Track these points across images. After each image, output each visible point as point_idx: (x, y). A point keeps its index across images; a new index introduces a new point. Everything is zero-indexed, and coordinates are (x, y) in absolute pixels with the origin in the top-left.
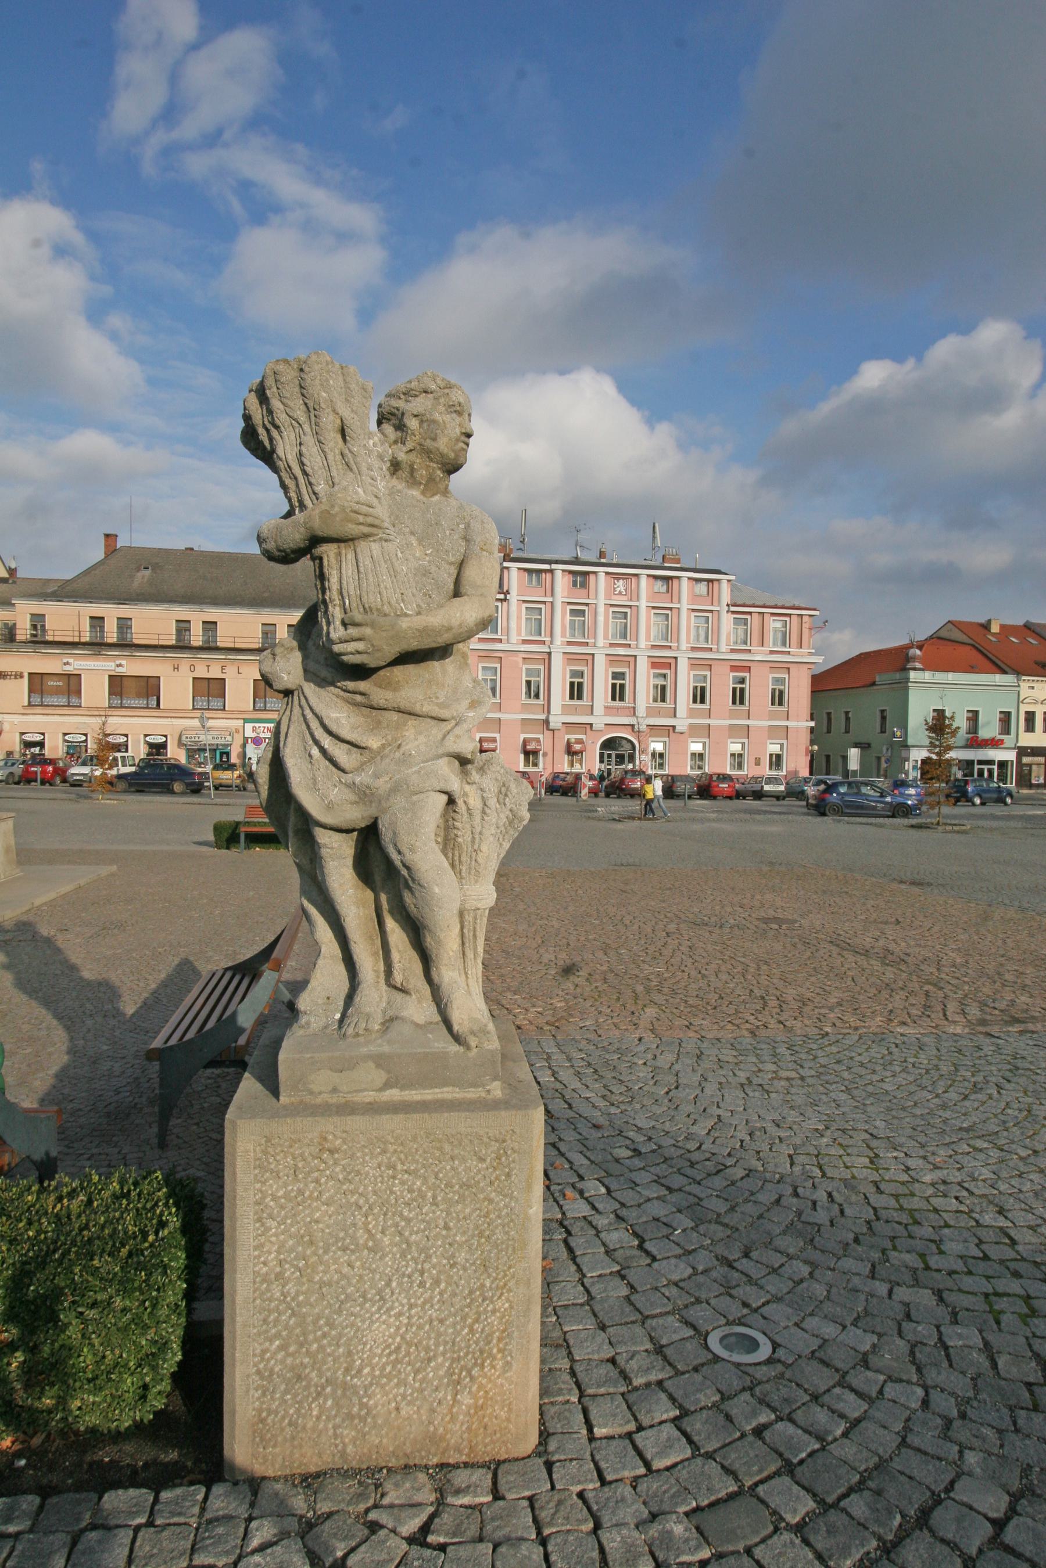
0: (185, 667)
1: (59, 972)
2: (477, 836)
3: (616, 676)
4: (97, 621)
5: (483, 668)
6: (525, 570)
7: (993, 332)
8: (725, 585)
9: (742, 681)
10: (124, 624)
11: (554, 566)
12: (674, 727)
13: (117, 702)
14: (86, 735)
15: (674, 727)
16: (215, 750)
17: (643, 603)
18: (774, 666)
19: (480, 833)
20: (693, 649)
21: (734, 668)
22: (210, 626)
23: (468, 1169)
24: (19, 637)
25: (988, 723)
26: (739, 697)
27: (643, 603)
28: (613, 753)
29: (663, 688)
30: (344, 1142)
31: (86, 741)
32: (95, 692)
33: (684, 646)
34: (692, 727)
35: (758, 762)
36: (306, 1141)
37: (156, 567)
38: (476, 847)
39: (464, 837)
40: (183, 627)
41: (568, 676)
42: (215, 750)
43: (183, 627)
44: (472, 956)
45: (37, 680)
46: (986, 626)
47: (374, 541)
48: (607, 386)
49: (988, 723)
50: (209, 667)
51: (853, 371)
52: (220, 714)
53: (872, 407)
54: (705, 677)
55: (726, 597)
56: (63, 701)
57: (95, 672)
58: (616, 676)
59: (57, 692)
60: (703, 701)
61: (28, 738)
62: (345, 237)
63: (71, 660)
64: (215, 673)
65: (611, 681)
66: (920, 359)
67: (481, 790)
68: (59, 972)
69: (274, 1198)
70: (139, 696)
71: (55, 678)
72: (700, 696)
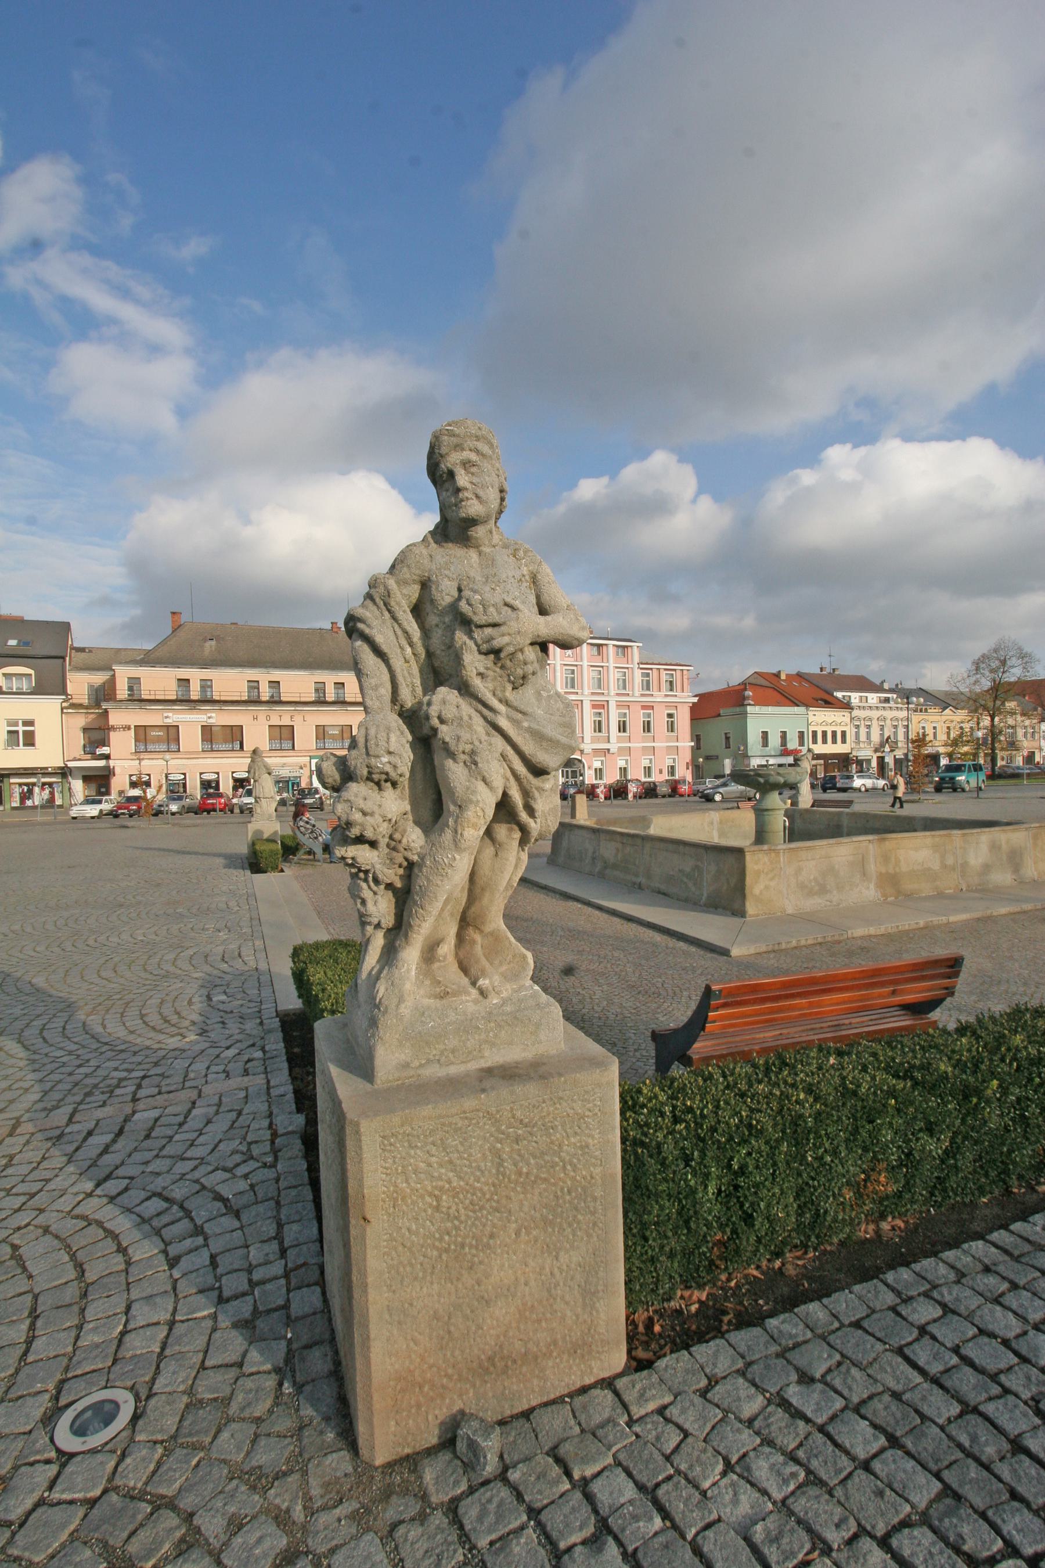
0: (262, 717)
4: (184, 682)
7: (660, 458)
8: (635, 650)
9: (649, 715)
10: (206, 684)
12: (609, 750)
13: (208, 746)
14: (184, 774)
15: (609, 750)
16: (288, 782)
17: (585, 663)
18: (668, 704)
20: (618, 694)
21: (644, 707)
22: (275, 684)
24: (119, 697)
25: (791, 740)
26: (647, 727)
27: (585, 663)
28: (570, 770)
29: (600, 722)
31: (185, 778)
32: (191, 739)
33: (612, 693)
34: (620, 748)
35: (661, 772)
37: (218, 639)
40: (254, 685)
42: (288, 782)
43: (254, 685)
45: (142, 730)
46: (777, 675)
48: (380, 483)
49: (791, 740)
50: (281, 717)
51: (573, 485)
52: (291, 753)
53: (587, 513)
54: (625, 714)
55: (636, 659)
56: (164, 747)
57: (190, 722)
59: (158, 740)
60: (624, 731)
61: (205, 777)
62: (155, 350)
63: (170, 714)
64: (286, 721)
66: (614, 474)
70: (225, 741)
71: (157, 729)
72: (623, 727)
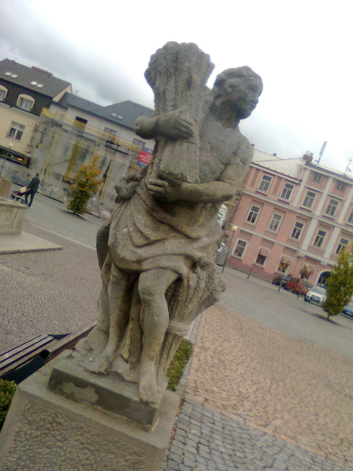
1: (14, 286)
2: (189, 300)
3: (344, 241)
5: (275, 215)
6: (314, 172)
11: (330, 175)
19: (191, 299)
23: (118, 462)
30: (66, 421)
36: (49, 413)
38: (186, 304)
39: (182, 296)
41: (317, 233)
44: (166, 357)
47: (186, 142)
58: (344, 241)
65: (339, 243)
67: (199, 277)
68: (14, 286)
69: (25, 434)
